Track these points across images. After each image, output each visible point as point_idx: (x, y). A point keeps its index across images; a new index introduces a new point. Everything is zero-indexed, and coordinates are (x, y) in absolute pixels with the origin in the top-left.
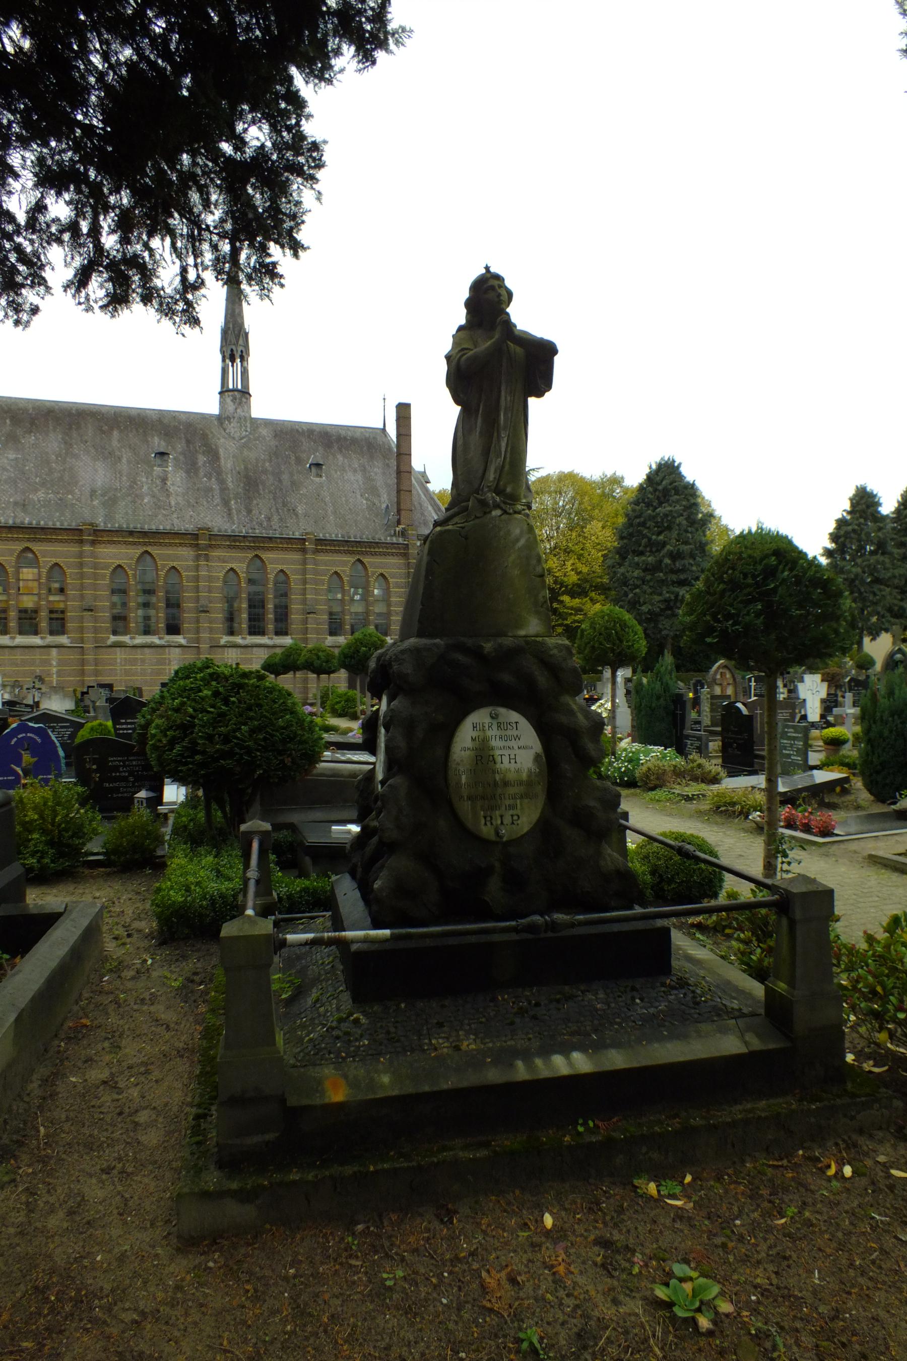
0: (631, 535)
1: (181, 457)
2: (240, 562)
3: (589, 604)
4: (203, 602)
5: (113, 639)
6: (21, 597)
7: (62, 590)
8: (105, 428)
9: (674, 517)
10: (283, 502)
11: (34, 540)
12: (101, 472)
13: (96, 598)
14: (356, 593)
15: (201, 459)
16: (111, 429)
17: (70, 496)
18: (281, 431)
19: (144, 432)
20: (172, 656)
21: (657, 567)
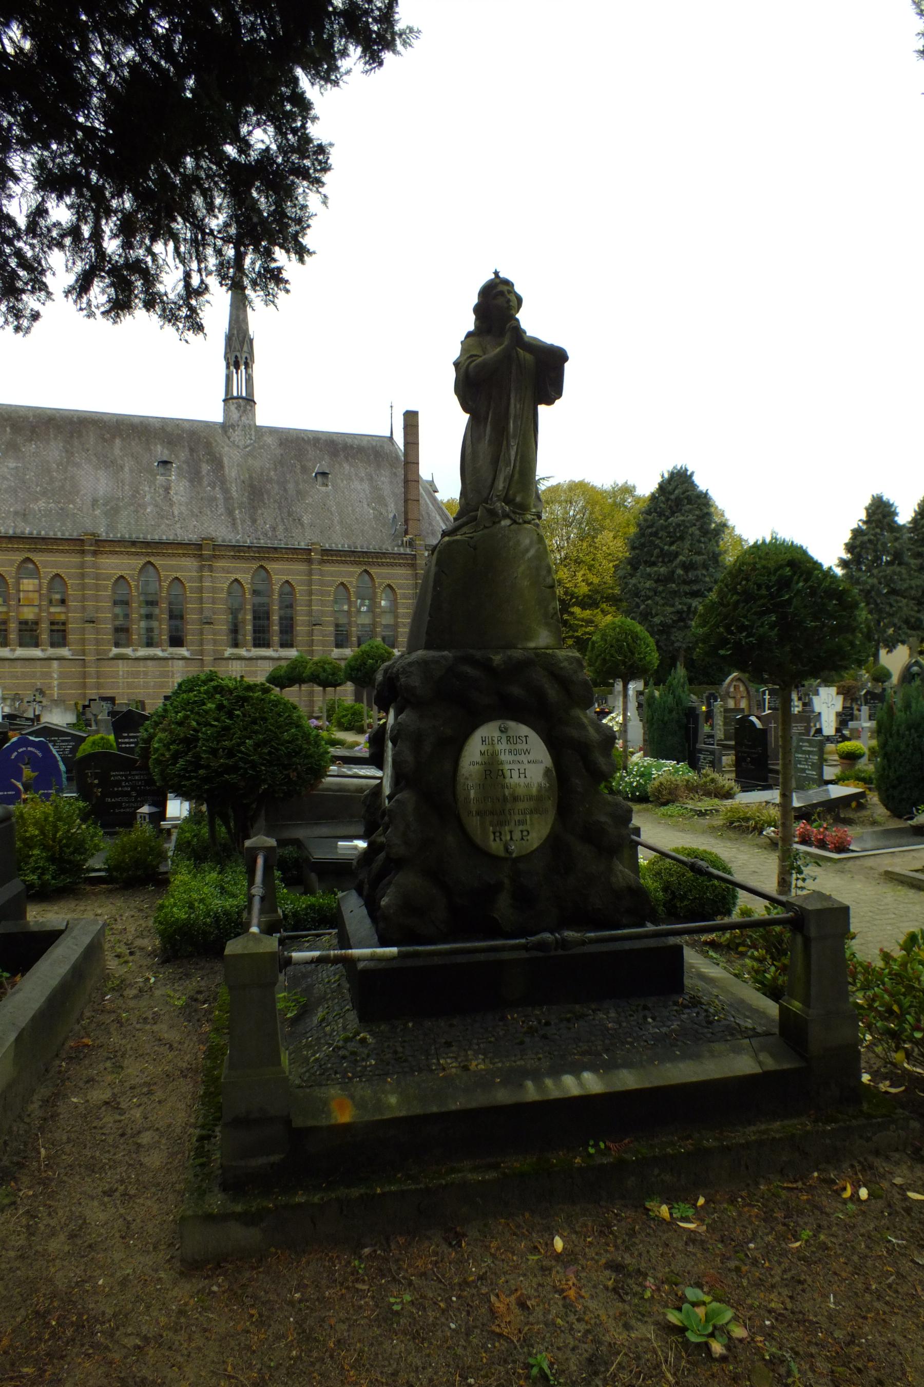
0: (643, 545)
1: (185, 466)
2: (244, 573)
3: (600, 616)
4: (206, 613)
5: (115, 651)
6: (21, 609)
7: (63, 602)
8: (107, 436)
9: (686, 527)
10: (289, 512)
11: (35, 550)
12: (103, 481)
13: (97, 609)
14: (362, 605)
15: (205, 468)
16: (114, 437)
17: (71, 506)
18: (287, 439)
19: (147, 440)
20: (175, 669)
21: (669, 578)
